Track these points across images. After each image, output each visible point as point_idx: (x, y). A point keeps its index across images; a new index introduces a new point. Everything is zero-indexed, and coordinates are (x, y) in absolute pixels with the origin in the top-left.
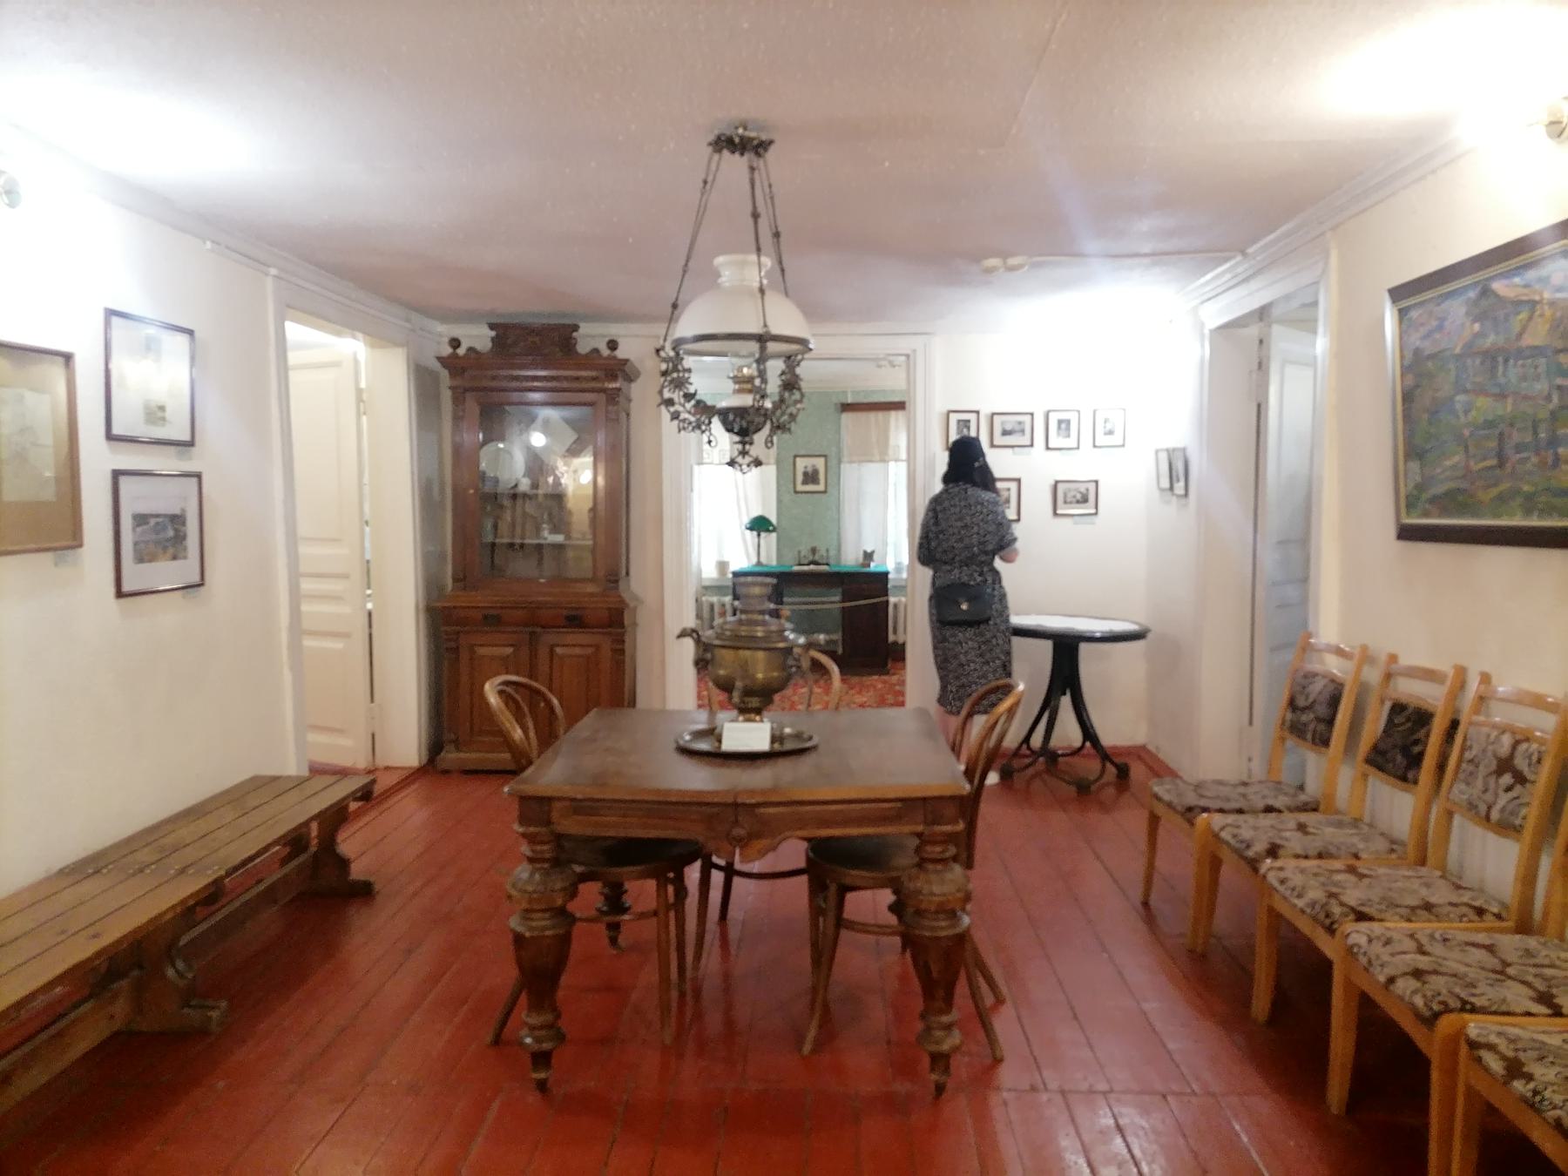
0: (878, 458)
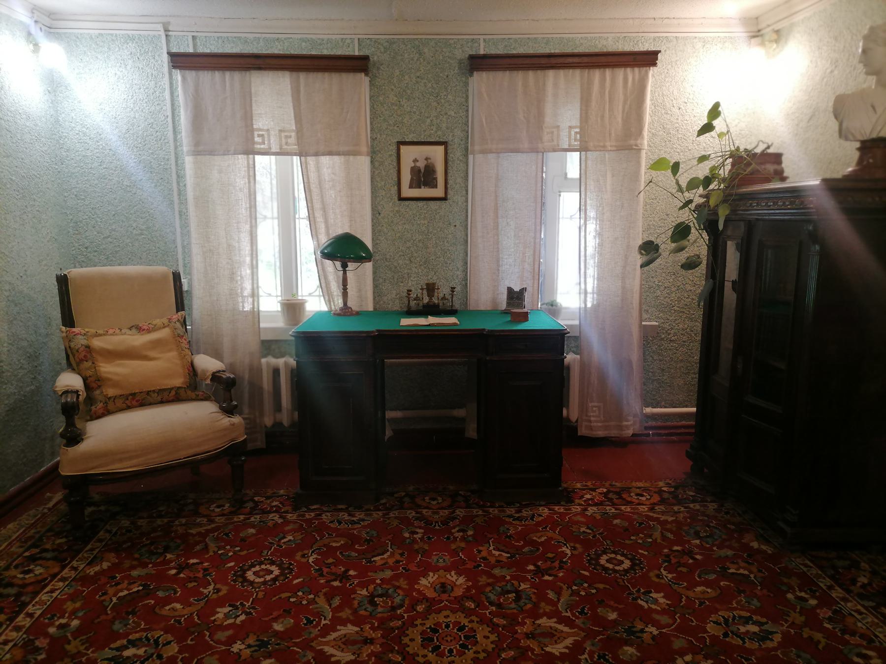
0: (526, 145)
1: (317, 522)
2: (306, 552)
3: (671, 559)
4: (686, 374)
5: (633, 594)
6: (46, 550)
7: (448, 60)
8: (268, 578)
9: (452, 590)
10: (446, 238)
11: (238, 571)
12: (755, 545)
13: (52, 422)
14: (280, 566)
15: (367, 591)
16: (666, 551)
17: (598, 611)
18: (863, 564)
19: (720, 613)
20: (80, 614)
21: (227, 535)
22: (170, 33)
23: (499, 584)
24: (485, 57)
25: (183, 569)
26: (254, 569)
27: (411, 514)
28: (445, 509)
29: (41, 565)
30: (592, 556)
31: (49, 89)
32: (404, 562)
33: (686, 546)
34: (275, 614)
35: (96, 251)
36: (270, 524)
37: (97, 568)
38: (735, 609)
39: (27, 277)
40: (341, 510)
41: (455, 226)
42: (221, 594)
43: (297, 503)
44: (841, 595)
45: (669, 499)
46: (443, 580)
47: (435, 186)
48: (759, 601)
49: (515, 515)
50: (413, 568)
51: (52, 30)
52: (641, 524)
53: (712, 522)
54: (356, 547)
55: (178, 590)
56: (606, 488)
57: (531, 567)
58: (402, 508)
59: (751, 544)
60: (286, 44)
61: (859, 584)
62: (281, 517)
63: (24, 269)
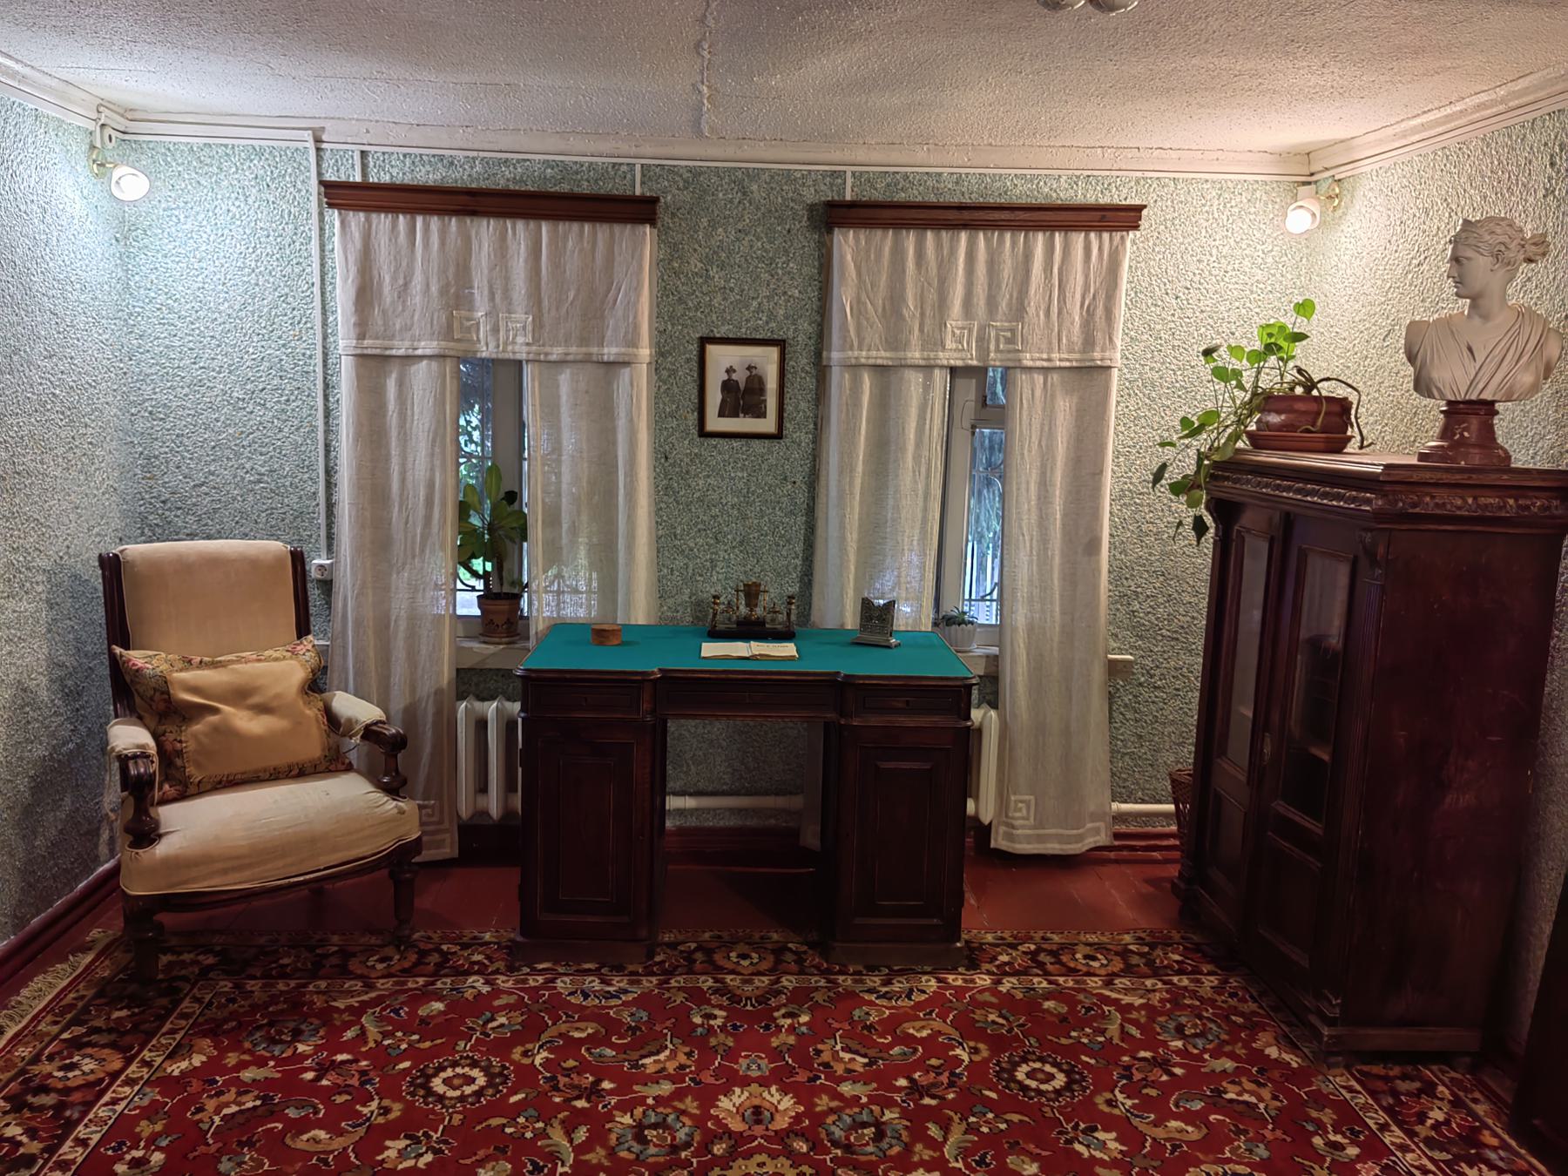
1: (547, 993)
2: (529, 1046)
3: (1132, 1074)
4: (1179, 744)
5: (1067, 1133)
6: (97, 1030)
7: (792, 204)
8: (468, 1090)
9: (772, 1119)
10: (779, 502)
11: (418, 1077)
12: (1273, 1052)
13: (97, 803)
14: (486, 1071)
15: (632, 1116)
16: (1126, 1059)
17: (1008, 1161)
18: (1441, 1088)
19: (1202, 1168)
20: (164, 1143)
21: (396, 1012)
22: (324, 146)
23: (848, 1111)
24: (853, 205)
25: (327, 1070)
26: (443, 1075)
27: (707, 983)
28: (763, 974)
29: (91, 1056)
30: (1004, 1065)
31: (118, 235)
32: (693, 1068)
33: (1160, 1051)
34: (481, 1154)
35: (180, 508)
36: (469, 994)
37: (184, 1065)
38: (1228, 1161)
39: (70, 558)
40: (588, 972)
41: (794, 483)
42: (392, 1116)
43: (515, 957)
44: (1398, 1141)
45: (1138, 965)
46: (757, 1102)
47: (762, 415)
48: (1266, 1149)
49: (880, 989)
50: (707, 1078)
51: (126, 137)
52: (1089, 1009)
53: (1207, 1010)
54: (613, 1039)
55: (321, 1106)
56: (1035, 944)
57: (902, 1082)
58: (691, 972)
59: (1267, 1051)
60: (519, 170)
61: (1429, 1122)
62: (487, 982)
63: (66, 543)
